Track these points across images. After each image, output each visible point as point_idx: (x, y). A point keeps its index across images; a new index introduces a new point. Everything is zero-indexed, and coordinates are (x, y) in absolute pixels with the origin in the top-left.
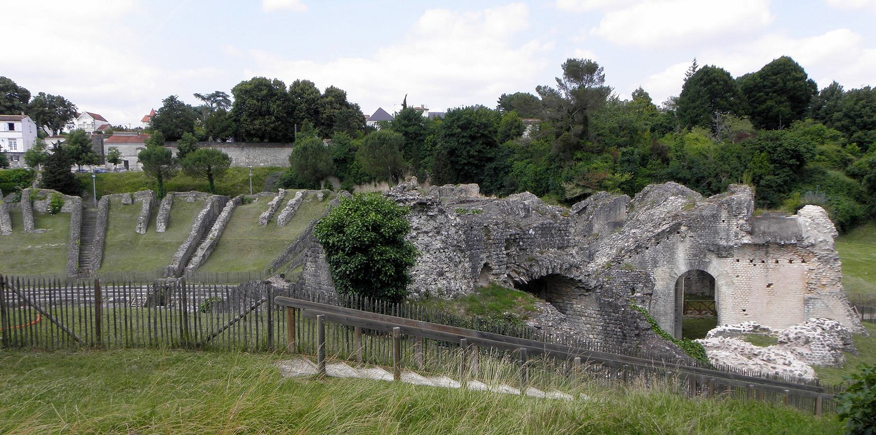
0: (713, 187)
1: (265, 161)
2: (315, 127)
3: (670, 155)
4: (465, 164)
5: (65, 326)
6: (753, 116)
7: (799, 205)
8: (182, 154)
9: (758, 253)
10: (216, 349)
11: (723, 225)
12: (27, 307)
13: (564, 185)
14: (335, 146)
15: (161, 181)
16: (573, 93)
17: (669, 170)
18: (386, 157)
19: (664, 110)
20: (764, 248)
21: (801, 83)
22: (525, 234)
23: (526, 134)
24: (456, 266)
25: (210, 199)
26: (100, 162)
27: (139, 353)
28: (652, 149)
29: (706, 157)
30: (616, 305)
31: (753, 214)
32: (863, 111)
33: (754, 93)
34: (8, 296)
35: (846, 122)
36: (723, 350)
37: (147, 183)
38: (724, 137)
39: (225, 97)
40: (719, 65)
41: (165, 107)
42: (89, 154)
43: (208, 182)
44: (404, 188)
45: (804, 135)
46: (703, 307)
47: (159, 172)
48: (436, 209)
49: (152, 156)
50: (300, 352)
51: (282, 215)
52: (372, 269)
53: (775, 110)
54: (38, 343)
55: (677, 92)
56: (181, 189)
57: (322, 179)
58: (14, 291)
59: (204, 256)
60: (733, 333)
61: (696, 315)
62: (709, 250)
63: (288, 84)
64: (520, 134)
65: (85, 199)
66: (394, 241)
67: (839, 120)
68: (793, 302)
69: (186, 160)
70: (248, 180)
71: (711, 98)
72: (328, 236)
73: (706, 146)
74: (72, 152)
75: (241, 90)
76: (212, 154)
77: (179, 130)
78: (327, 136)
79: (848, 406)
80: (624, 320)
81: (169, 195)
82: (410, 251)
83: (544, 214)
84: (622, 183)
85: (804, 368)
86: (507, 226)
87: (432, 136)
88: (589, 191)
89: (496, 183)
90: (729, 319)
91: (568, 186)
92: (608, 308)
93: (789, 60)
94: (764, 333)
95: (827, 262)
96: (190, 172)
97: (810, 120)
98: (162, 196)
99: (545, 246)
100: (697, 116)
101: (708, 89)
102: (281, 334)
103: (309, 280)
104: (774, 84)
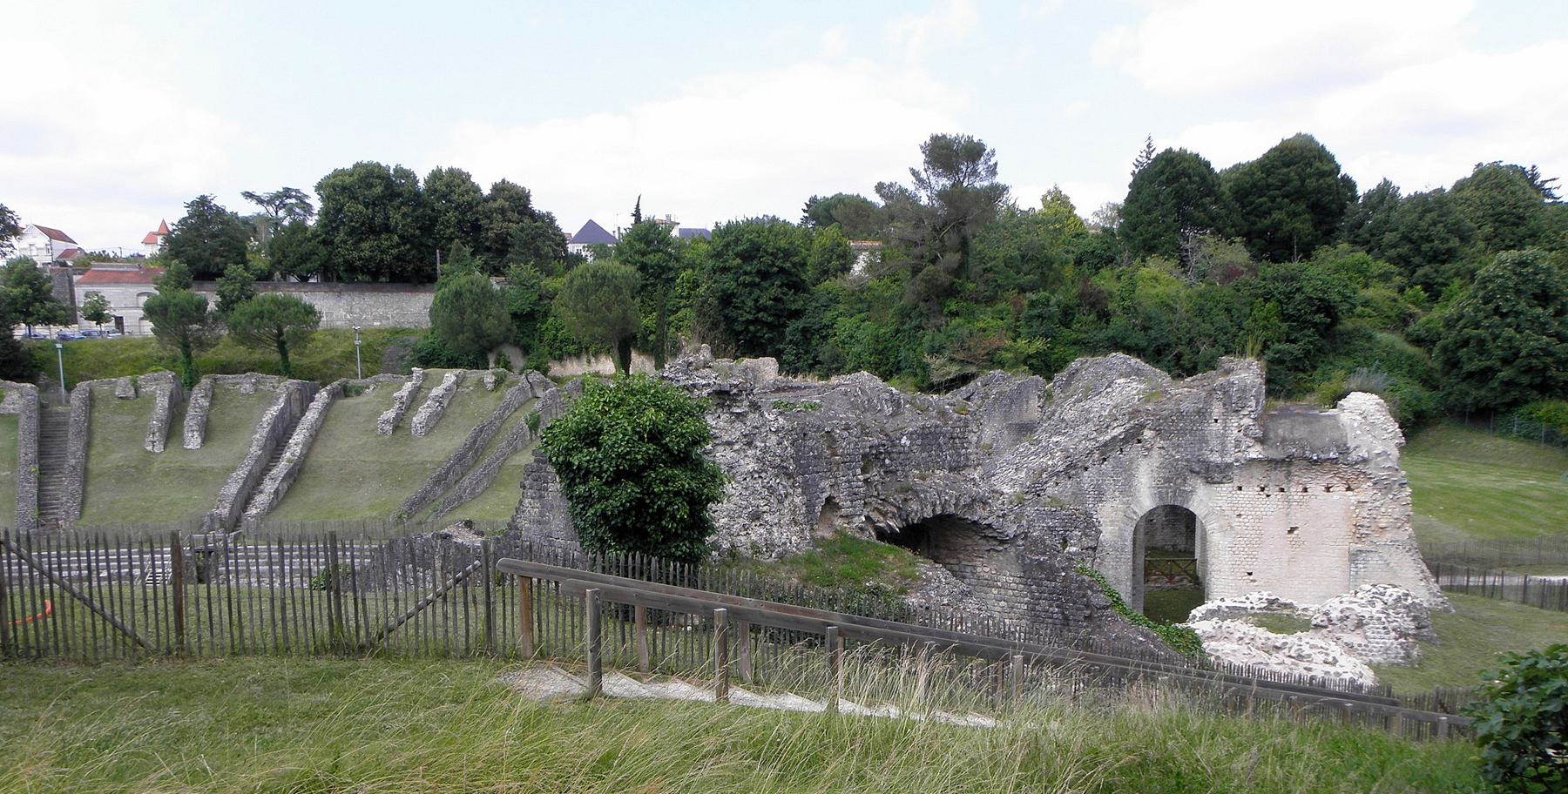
0: (1185, 362)
1: (381, 318)
2: (473, 254)
3: (1111, 306)
4: (748, 322)
5: (118, 619)
6: (1250, 238)
7: (1340, 391)
8: (226, 305)
9: (1273, 475)
10: (387, 655)
11: (1215, 427)
12: (47, 586)
13: (927, 359)
14: (513, 291)
15: (188, 355)
16: (942, 195)
17: (1110, 333)
18: (609, 310)
19: (1096, 226)
20: (1285, 465)
21: (1329, 180)
22: (894, 446)
23: (857, 268)
24: (780, 502)
25: (284, 388)
26: (69, 320)
27: (256, 662)
28: (1081, 295)
29: (1173, 310)
30: (1052, 567)
31: (1265, 410)
32: (1433, 231)
33: (1251, 198)
34: (9, 565)
35: (1404, 249)
36: (1230, 643)
37: (161, 359)
38: (1203, 276)
39: (301, 199)
40: (1192, 148)
41: (191, 217)
42: (48, 305)
43: (277, 357)
44: (690, 364)
45: (1337, 271)
46: (1176, 570)
47: (185, 337)
48: (746, 403)
49: (171, 309)
50: (542, 655)
51: (420, 417)
52: (645, 506)
53: (1286, 228)
54: (68, 650)
55: (1120, 195)
56: (226, 368)
57: (491, 350)
58: (20, 557)
59: (277, 492)
60: (1235, 613)
61: (1164, 583)
62: (1192, 471)
63: (422, 175)
64: (846, 269)
65: (43, 389)
66: (685, 459)
67: (1394, 246)
68: (1330, 557)
69: (235, 316)
70: (353, 353)
71: (1178, 206)
72: (569, 451)
73: (1172, 290)
74: (14, 301)
75: (334, 187)
76: (284, 305)
77: (218, 260)
78: (496, 271)
79: (1496, 721)
80: (1065, 591)
81: (205, 381)
82: (714, 477)
83: (924, 410)
84: (1030, 356)
85: (1358, 669)
86: (865, 431)
87: (690, 271)
88: (972, 369)
89: (807, 352)
90: (1224, 587)
91: (934, 362)
92: (1037, 572)
93: (1311, 139)
94: (1286, 612)
95: (1387, 488)
96: (244, 338)
97: (1345, 246)
98: (192, 383)
99: (928, 466)
100: (1154, 238)
101: (1174, 193)
102: (510, 621)
103: (528, 529)
104: (1285, 183)
